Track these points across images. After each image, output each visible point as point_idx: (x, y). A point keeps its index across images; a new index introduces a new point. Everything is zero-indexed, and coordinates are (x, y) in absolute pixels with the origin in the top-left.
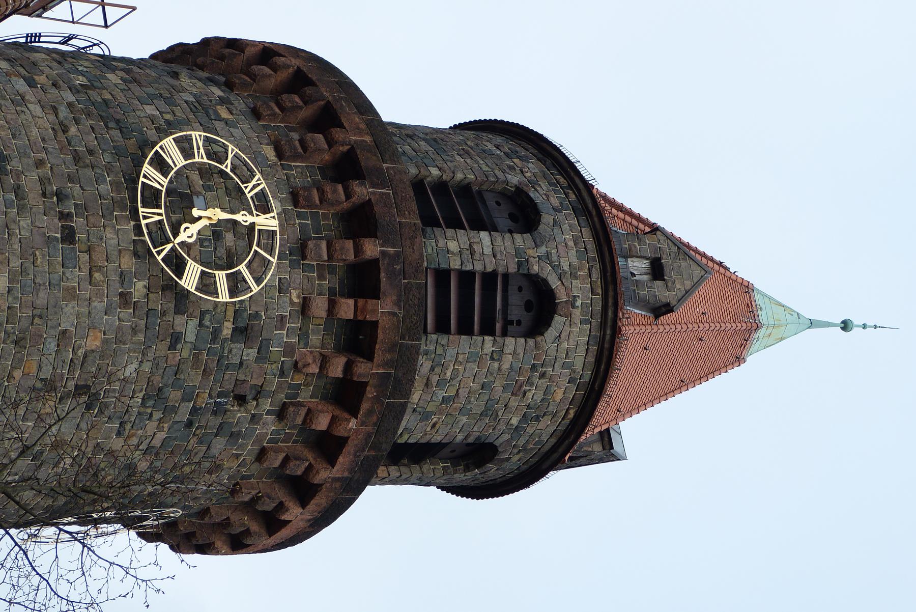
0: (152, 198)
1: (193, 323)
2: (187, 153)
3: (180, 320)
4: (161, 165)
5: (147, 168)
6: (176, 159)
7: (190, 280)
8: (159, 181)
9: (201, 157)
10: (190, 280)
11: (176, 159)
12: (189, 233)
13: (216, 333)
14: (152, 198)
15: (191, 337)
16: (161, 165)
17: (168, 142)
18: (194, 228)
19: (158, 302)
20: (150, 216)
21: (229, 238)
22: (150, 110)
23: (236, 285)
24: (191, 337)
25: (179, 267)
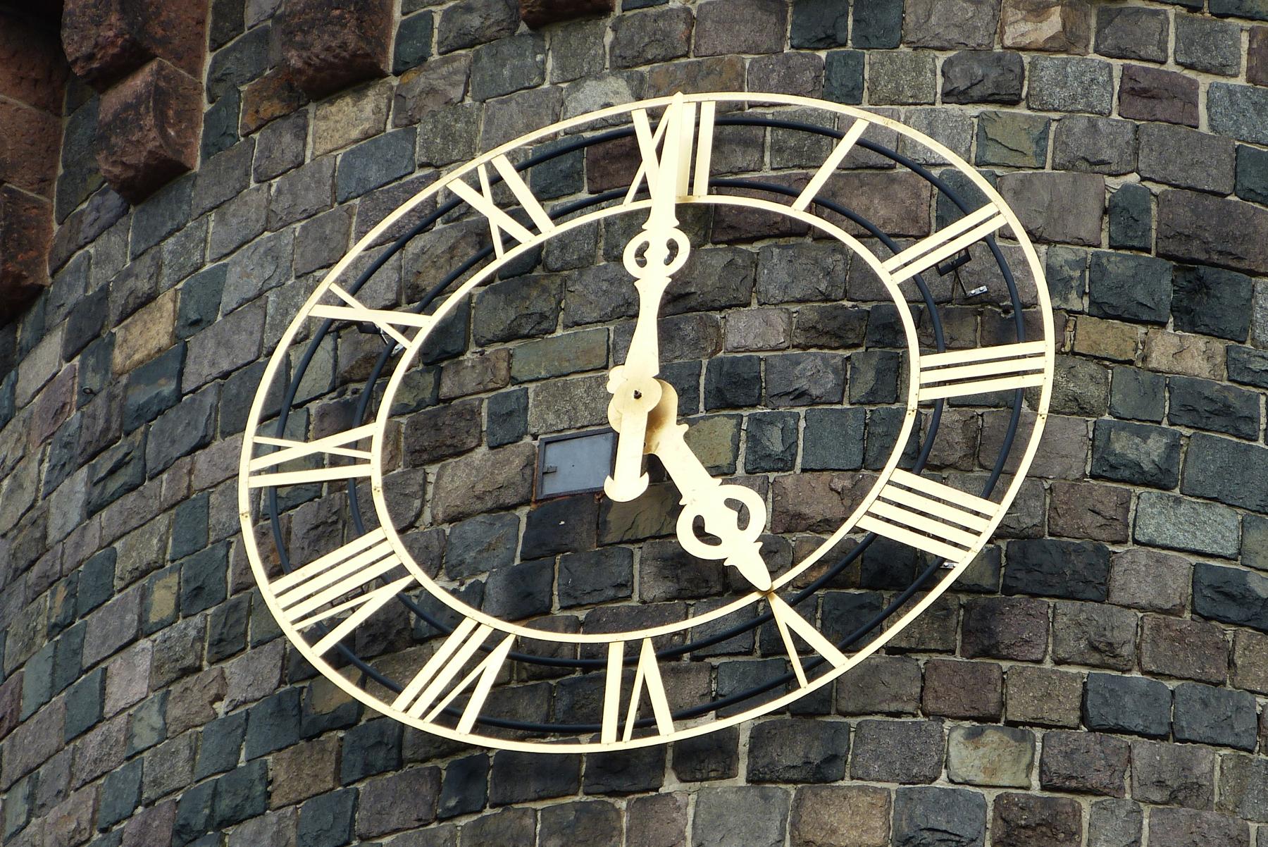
0: (552, 687)
1: (1153, 514)
2: (331, 516)
3: (1135, 578)
4: (395, 640)
5: (411, 707)
6: (369, 566)
7: (953, 525)
8: (471, 653)
9: (364, 452)
10: (953, 525)
11: (369, 566)
12: (724, 520)
13: (1205, 410)
14: (552, 687)
15: (1217, 529)
16: (395, 640)
17: (289, 601)
18: (702, 495)
19: (1044, 676)
20: (638, 695)
21: (750, 331)
22: (130, 681)
23: (974, 304)
24: (1217, 529)
25: (890, 571)
